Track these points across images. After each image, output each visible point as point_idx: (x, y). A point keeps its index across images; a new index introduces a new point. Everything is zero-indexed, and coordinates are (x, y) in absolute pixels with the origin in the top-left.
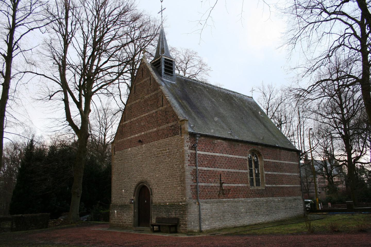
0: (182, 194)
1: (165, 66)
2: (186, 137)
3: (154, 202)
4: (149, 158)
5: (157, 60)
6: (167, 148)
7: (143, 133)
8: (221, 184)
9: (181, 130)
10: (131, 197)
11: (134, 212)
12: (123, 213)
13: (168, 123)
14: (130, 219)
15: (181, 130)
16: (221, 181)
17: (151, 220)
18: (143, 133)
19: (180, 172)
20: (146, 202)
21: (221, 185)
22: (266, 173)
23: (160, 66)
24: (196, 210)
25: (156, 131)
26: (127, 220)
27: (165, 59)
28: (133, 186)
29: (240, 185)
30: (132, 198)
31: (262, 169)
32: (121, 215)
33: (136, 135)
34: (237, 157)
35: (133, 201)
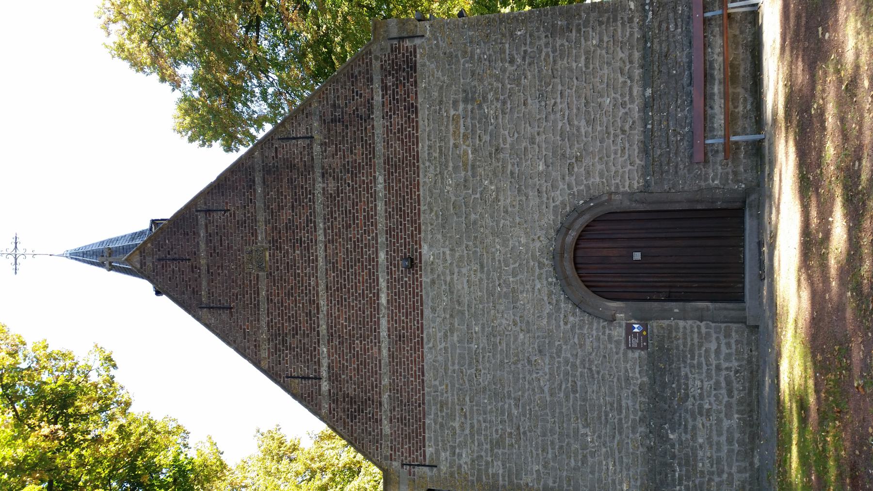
0: (615, 20)
4: (473, 217)
7: (382, 255)
10: (618, 343)
12: (689, 404)
13: (371, 108)
14: (713, 346)
17: (710, 189)
18: (382, 255)
30: (618, 333)
33: (383, 300)
35: (637, 328)
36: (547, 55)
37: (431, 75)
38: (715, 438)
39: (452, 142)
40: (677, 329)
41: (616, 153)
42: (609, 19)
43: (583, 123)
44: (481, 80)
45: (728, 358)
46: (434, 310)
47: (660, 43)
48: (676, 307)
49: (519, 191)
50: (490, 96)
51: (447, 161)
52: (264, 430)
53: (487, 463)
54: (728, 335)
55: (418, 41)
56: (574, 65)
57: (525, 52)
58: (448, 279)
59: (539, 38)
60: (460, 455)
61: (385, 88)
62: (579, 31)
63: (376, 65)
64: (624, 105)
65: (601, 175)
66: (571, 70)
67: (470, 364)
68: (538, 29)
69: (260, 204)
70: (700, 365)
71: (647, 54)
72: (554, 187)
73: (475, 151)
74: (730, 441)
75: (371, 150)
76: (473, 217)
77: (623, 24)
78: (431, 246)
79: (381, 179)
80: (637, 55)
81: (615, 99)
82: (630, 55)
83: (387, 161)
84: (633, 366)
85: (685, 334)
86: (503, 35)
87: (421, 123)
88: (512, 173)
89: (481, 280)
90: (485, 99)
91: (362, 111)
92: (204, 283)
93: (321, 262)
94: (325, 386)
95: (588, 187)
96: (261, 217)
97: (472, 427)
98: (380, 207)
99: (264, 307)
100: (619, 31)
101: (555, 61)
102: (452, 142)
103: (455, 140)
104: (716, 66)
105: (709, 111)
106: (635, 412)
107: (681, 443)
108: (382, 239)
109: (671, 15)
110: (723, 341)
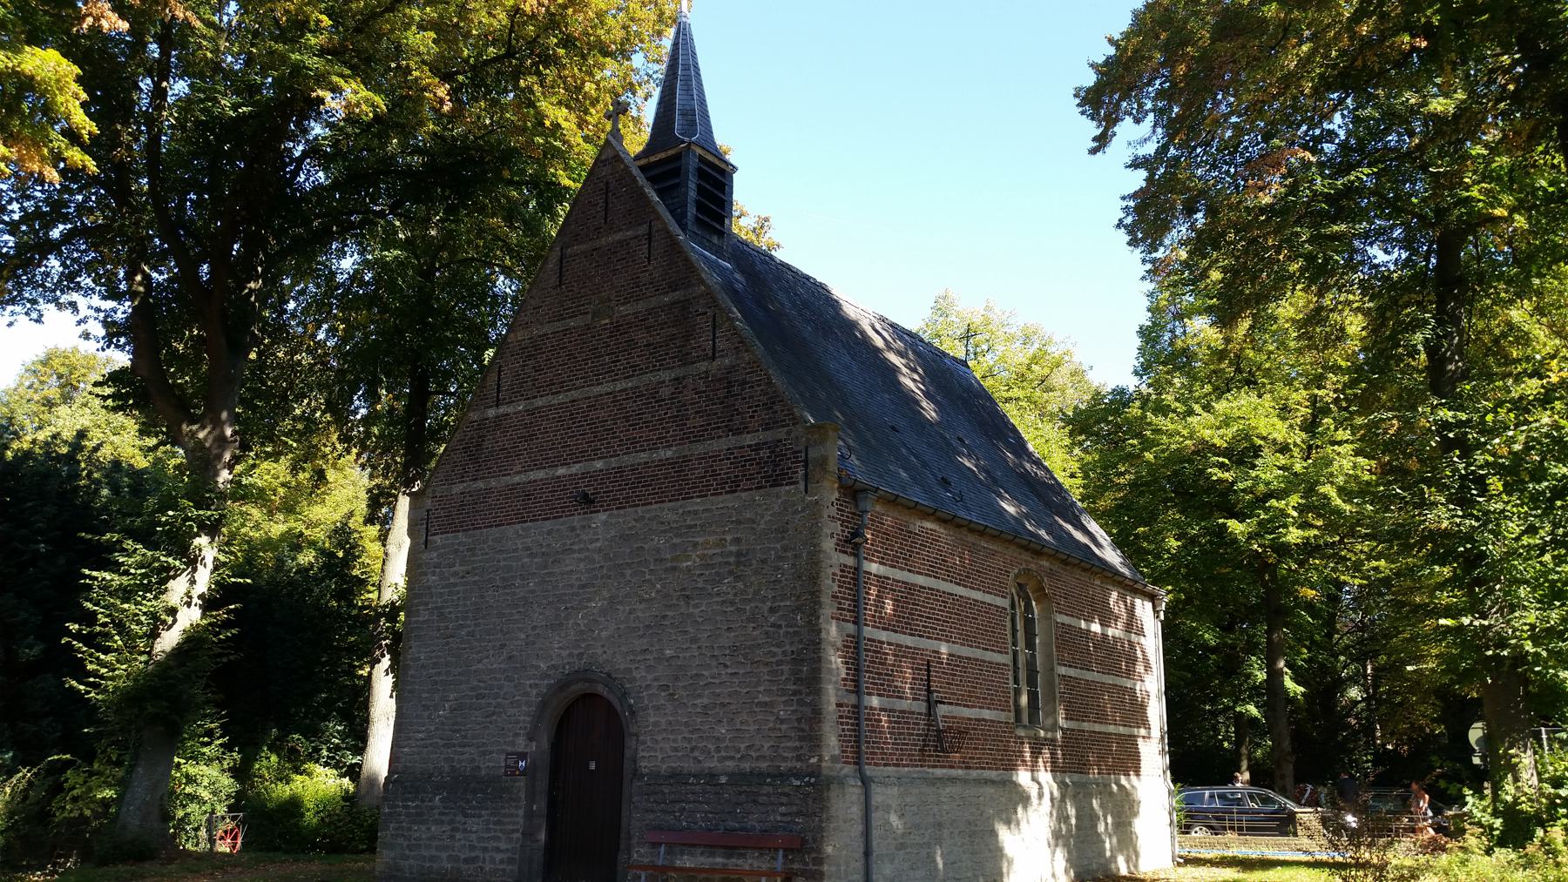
0: (801, 739)
1: (701, 190)
2: (830, 494)
3: (645, 771)
4: (628, 572)
5: (662, 155)
6: (729, 538)
7: (599, 465)
8: (931, 705)
9: (806, 466)
10: (513, 743)
11: (529, 815)
12: (460, 818)
13: (738, 432)
14: (503, 846)
15: (806, 466)
16: (929, 691)
17: (629, 850)
18: (599, 465)
19: (791, 644)
20: (593, 766)
21: (929, 708)
22: (1063, 670)
23: (676, 186)
24: (856, 811)
25: (670, 463)
26: (485, 849)
27: (702, 159)
28: (527, 694)
29: (987, 714)
30: (521, 744)
31: (1049, 656)
32: (446, 828)
33: (561, 471)
34: (978, 595)
35: (522, 764)
36: (774, 655)
37: (765, 506)
38: (434, 844)
39: (700, 540)
40: (517, 808)
41: (675, 741)
42: (803, 730)
43: (706, 701)
44: (756, 572)
45: (493, 860)
46: (549, 533)
47: (768, 795)
48: (540, 806)
49: (648, 627)
50: (740, 585)
51: (681, 536)
52: (1093, 129)
53: (426, 604)
54: (511, 861)
55: (802, 486)
56: (761, 689)
57: (780, 626)
58: (576, 547)
59: (791, 644)
60: (434, 574)
61: (757, 448)
62: (795, 693)
63: (781, 433)
64: (718, 750)
65: (656, 724)
66: (758, 683)
67: (503, 579)
68: (801, 641)
69: (654, 302)
70: (488, 830)
71: (758, 777)
72: (649, 668)
73: (689, 569)
74: (432, 859)
75: (697, 438)
76: (628, 572)
77: (796, 748)
78: (605, 523)
79: (669, 454)
80: (764, 765)
81: (724, 739)
82: (764, 757)
83: (686, 459)
84: (494, 763)
85: (512, 815)
86: (798, 598)
87: (720, 498)
88: (664, 617)
89: (572, 586)
90: (738, 578)
91: (737, 420)
92: (583, 247)
93: (597, 390)
94: (491, 413)
95: (646, 708)
96: (641, 306)
97: (455, 585)
98: (644, 456)
99: (559, 326)
100: (789, 744)
101: (767, 664)
102: (700, 540)
103: (1508, 428)
104: (740, 862)
105: (699, 851)
106: (460, 761)
107: (432, 808)
108: (614, 462)
109: (795, 809)
110: (504, 856)
